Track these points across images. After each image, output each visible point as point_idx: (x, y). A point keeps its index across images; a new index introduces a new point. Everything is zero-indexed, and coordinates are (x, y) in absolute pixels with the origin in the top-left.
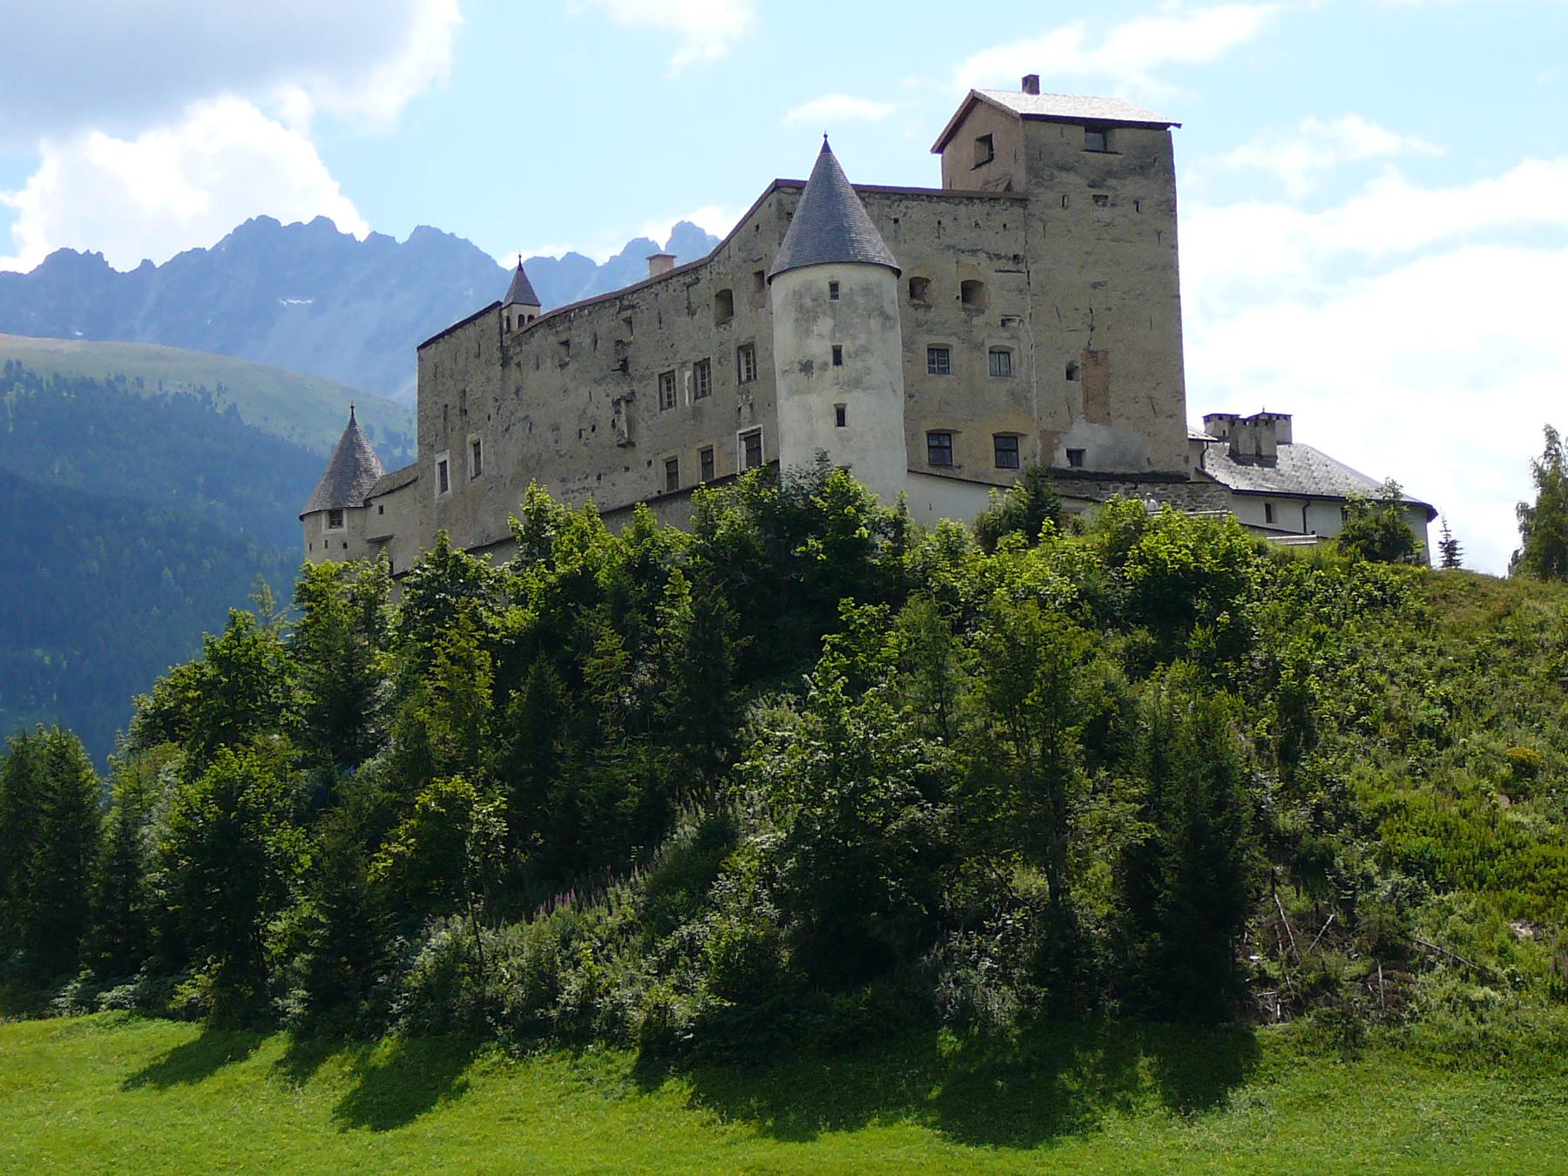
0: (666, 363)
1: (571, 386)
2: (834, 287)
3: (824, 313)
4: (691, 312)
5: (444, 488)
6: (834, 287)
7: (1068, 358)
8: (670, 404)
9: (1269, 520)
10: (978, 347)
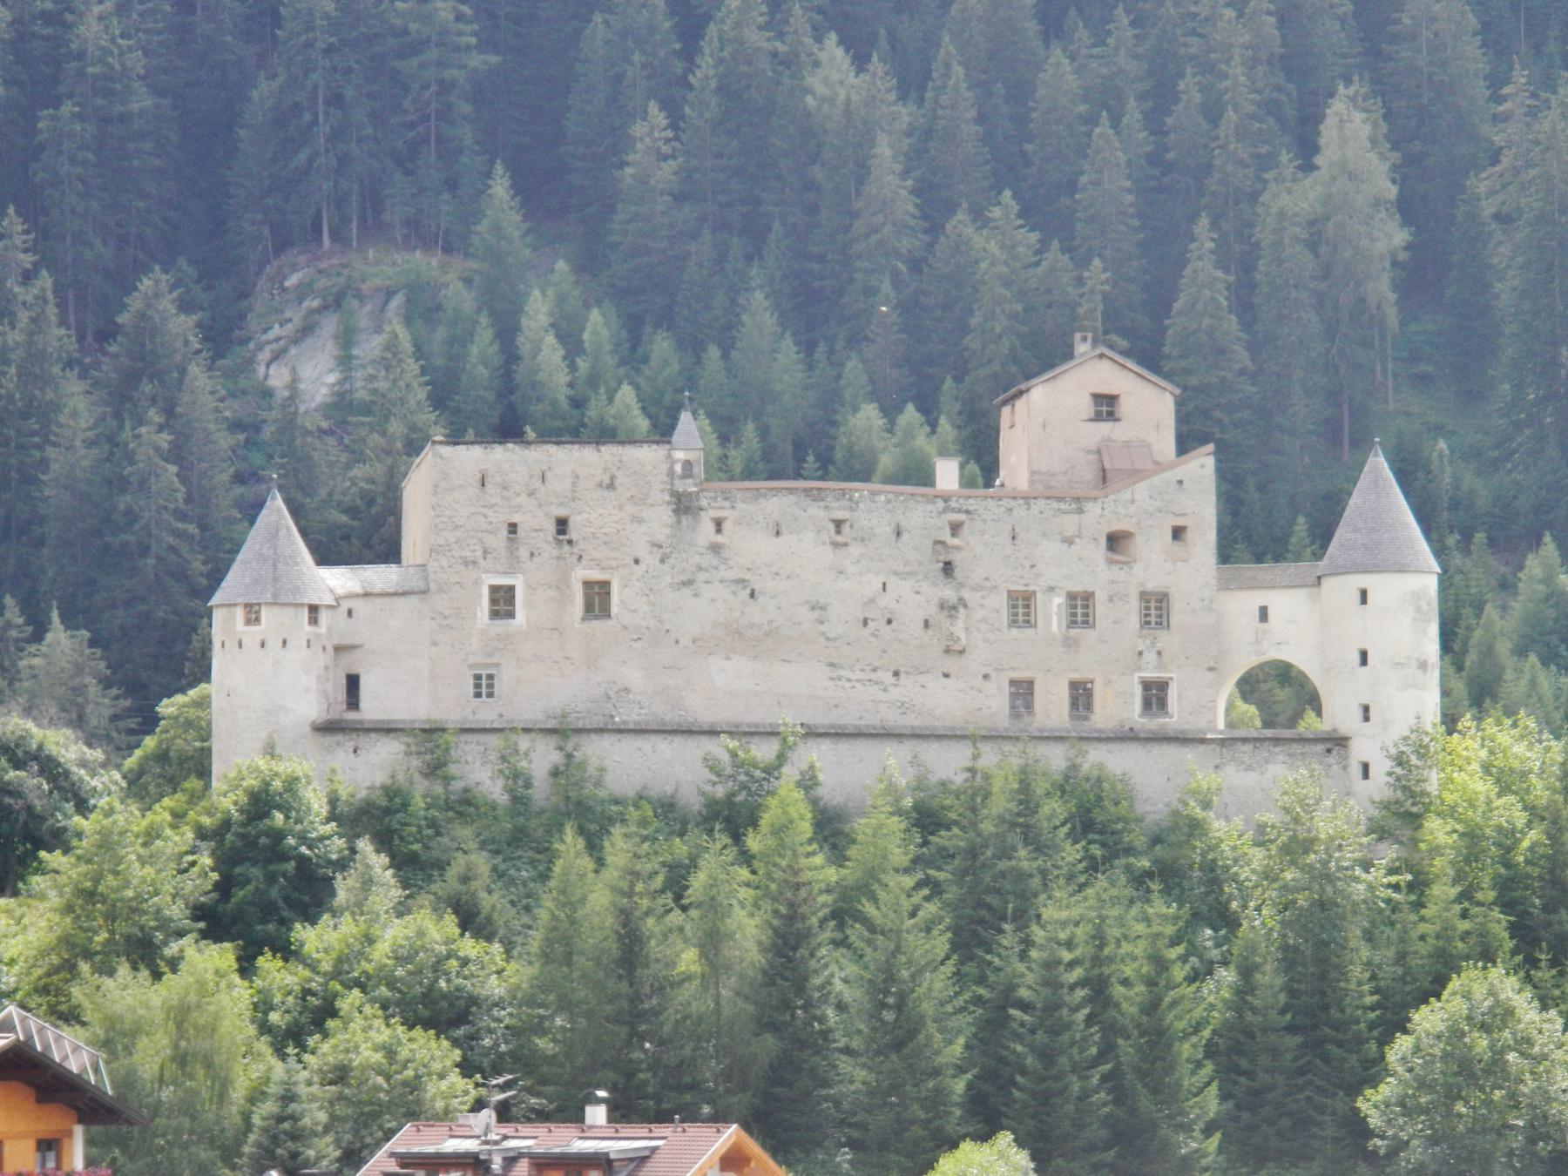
1: (851, 569)
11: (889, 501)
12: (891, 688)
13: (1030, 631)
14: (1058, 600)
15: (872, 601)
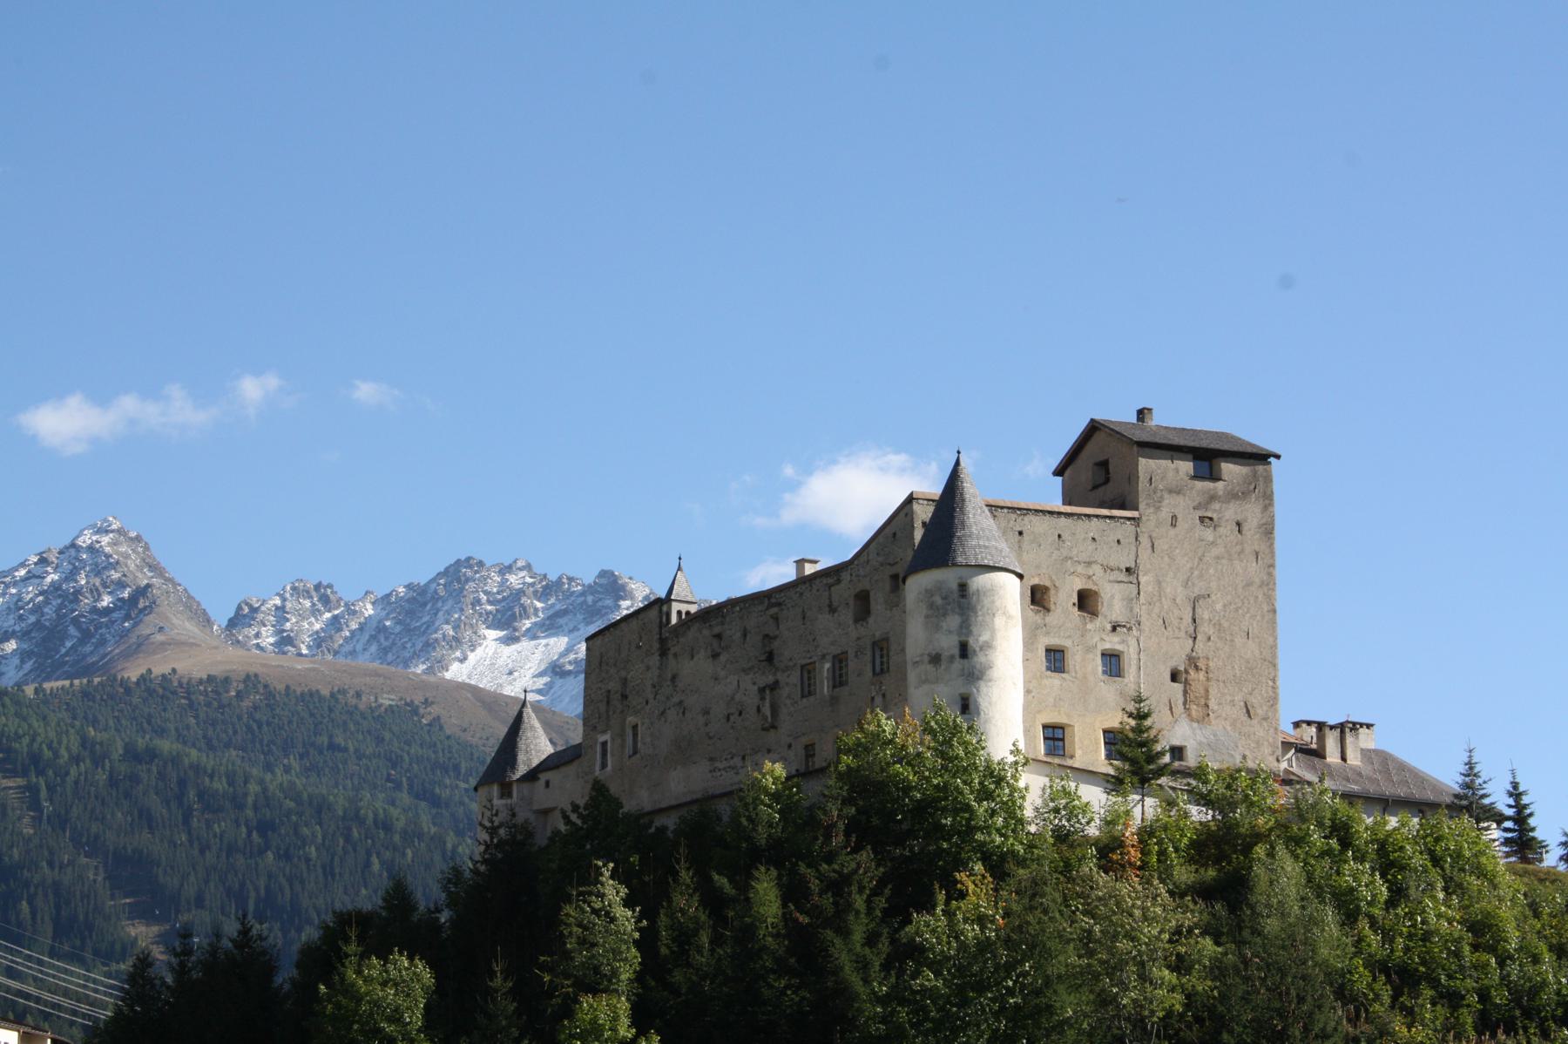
1: (722, 673)
5: (604, 765)
13: (812, 699)
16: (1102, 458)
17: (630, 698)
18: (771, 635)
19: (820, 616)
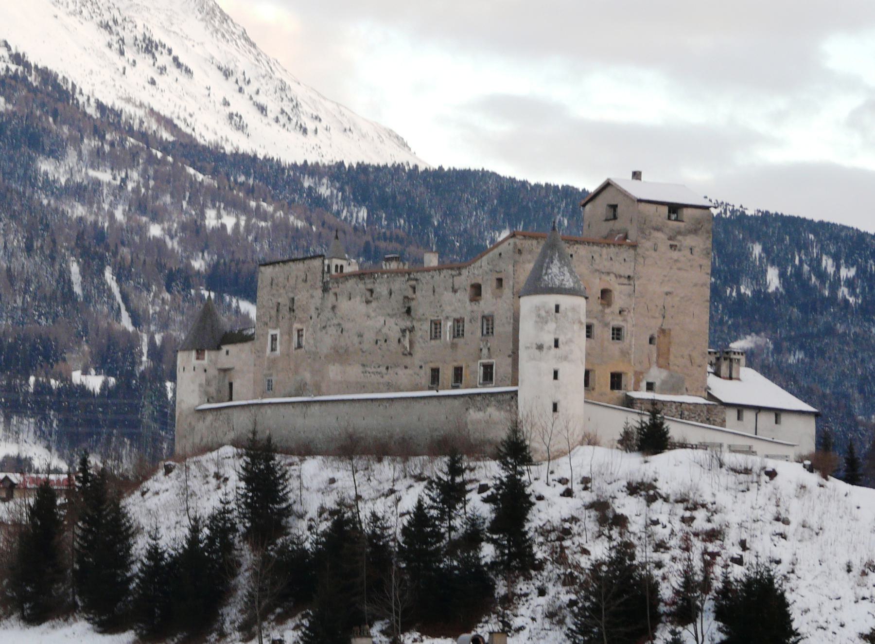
0: (436, 315)
1: (373, 314)
2: (557, 308)
3: (552, 320)
4: (455, 291)
5: (273, 349)
6: (557, 308)
7: (651, 333)
8: (436, 336)
9: (756, 434)
10: (606, 325)
11: (388, 277)
12: (385, 376)
13: (438, 341)
14: (450, 324)
15: (380, 330)
16: (613, 203)
17: (296, 311)
18: (409, 297)
19: (445, 293)
